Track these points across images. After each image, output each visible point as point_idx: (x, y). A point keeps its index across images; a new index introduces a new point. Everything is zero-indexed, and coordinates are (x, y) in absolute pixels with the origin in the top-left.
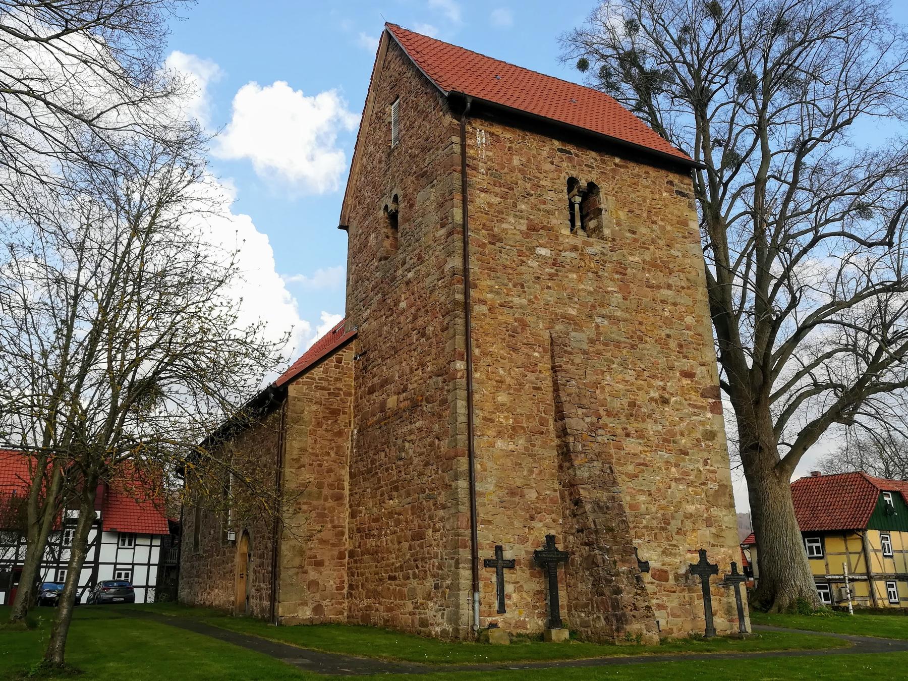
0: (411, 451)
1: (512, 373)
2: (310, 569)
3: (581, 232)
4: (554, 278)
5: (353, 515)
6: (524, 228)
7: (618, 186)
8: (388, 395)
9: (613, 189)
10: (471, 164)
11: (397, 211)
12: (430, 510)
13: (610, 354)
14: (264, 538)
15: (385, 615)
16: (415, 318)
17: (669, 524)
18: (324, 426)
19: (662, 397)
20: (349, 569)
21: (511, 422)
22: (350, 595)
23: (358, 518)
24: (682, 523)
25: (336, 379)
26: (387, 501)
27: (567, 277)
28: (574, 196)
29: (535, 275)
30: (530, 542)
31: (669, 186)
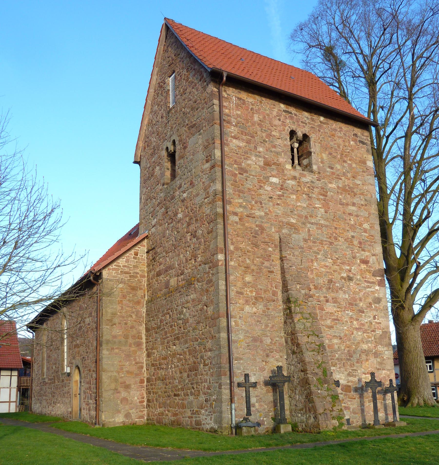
0: (187, 314)
1: (255, 262)
2: (121, 389)
3: (298, 167)
4: (282, 198)
5: (149, 355)
6: (262, 164)
7: (322, 136)
8: (171, 277)
9: (319, 139)
10: (226, 119)
11: (175, 152)
12: (201, 352)
13: (316, 248)
14: (90, 371)
15: (173, 418)
16: (189, 225)
17: (352, 357)
18: (128, 298)
19: (348, 276)
20: (147, 389)
21: (254, 294)
22: (148, 406)
23: (152, 357)
24: (360, 356)
25: (134, 267)
26: (171, 347)
27: (290, 197)
28: (294, 143)
29: (269, 196)
30: (267, 370)
31: (355, 137)
